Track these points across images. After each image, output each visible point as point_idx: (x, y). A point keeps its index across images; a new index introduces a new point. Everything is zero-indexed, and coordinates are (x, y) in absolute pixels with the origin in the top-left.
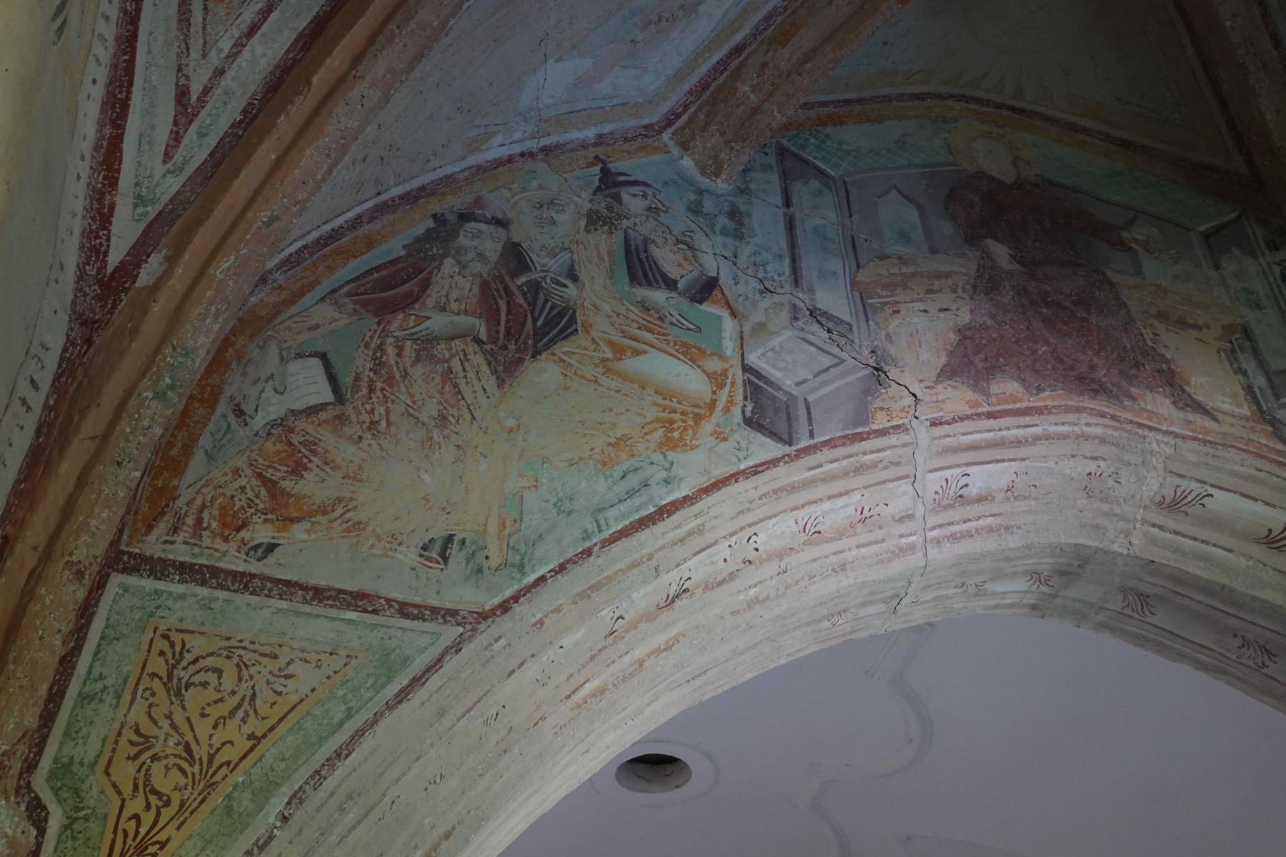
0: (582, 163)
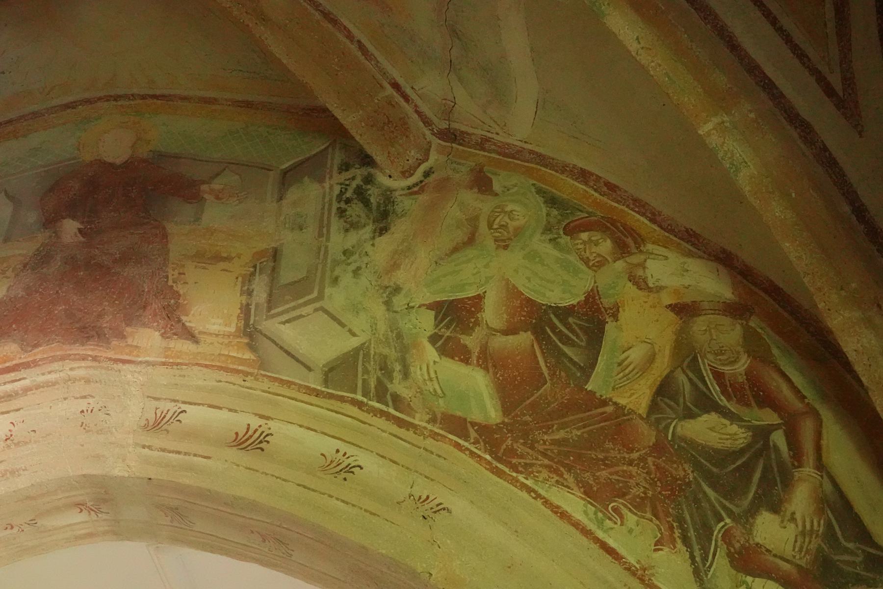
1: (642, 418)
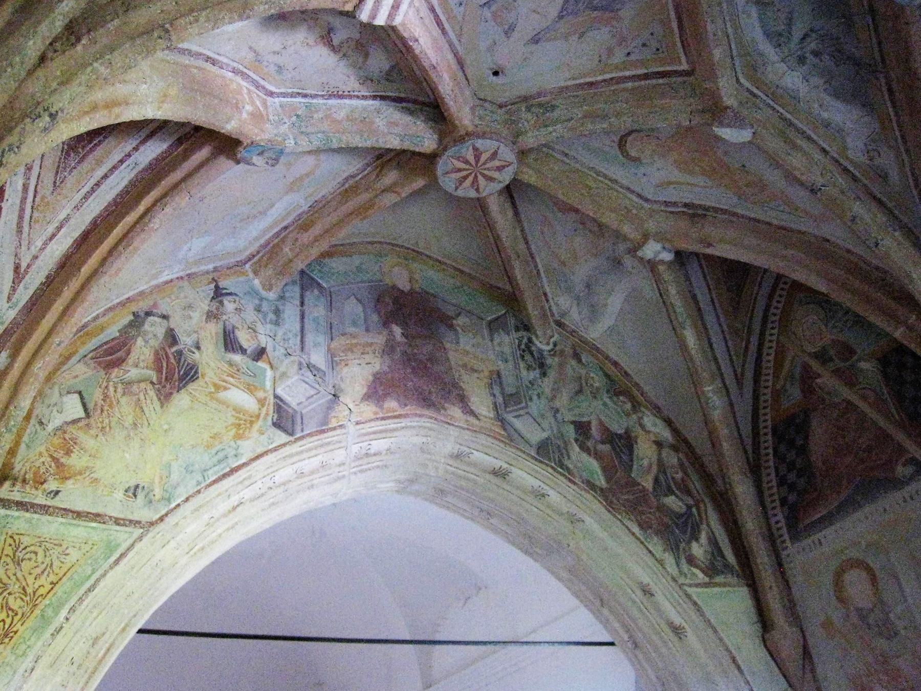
0: (206, 282)
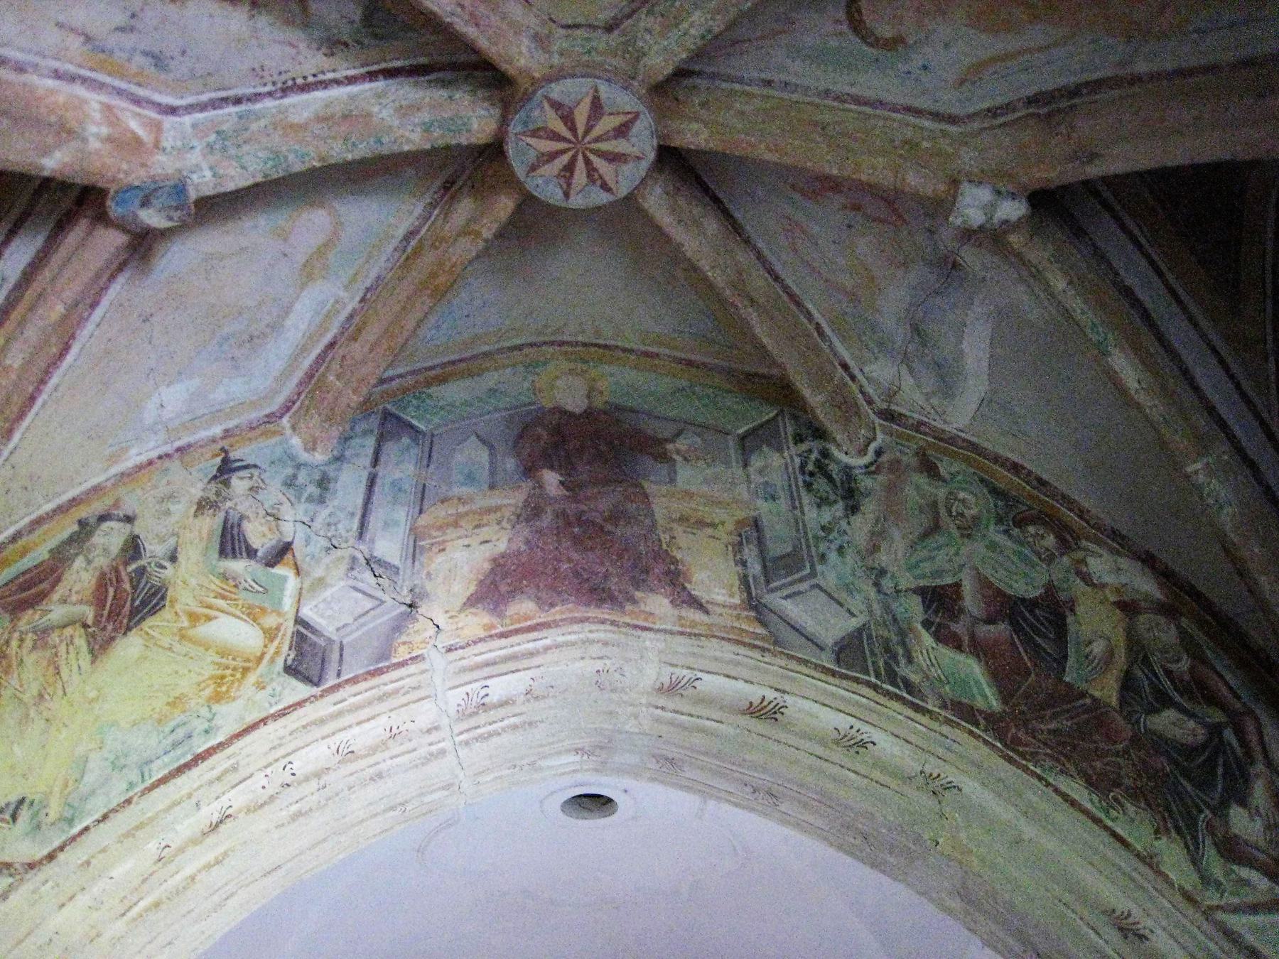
0: (208, 455)
1: (1114, 709)
